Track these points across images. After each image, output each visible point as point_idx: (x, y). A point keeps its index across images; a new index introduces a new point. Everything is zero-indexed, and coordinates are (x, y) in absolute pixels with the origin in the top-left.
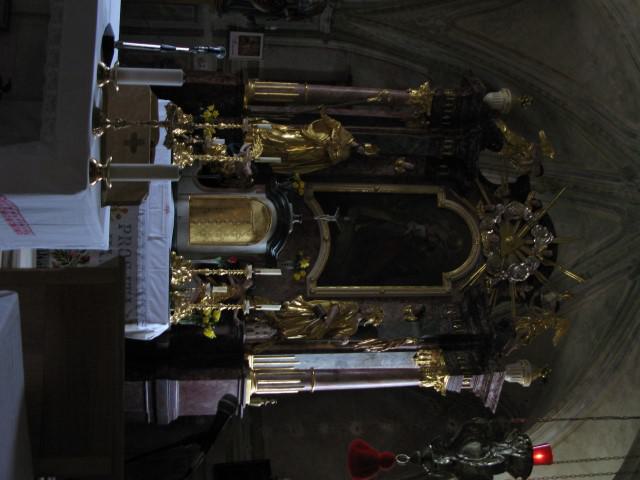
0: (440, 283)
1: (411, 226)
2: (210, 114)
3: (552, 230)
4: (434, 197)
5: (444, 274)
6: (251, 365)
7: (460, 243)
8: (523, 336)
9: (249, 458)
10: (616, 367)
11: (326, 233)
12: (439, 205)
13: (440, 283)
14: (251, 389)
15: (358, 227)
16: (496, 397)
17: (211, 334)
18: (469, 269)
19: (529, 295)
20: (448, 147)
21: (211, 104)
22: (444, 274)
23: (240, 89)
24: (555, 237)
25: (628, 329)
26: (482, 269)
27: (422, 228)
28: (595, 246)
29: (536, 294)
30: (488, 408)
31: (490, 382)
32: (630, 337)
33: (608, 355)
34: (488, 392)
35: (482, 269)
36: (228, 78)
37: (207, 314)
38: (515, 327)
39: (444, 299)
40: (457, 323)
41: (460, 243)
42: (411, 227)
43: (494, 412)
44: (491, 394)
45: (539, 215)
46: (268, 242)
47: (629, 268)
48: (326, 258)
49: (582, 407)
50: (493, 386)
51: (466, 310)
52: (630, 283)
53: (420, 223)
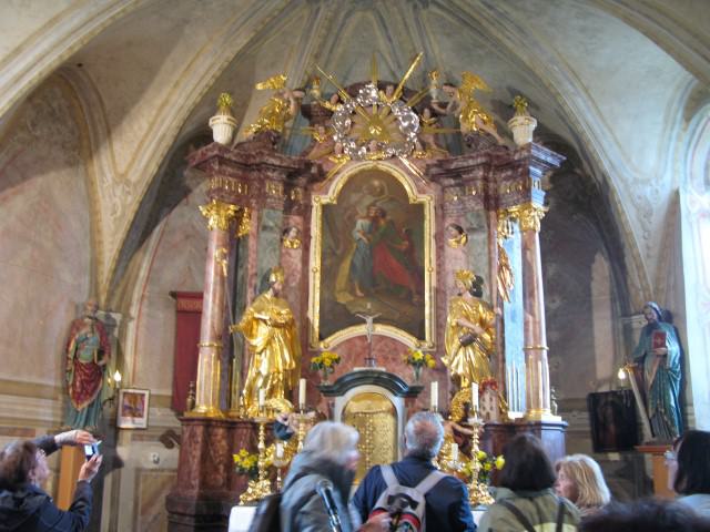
0: (421, 207)
1: (358, 235)
2: (246, 461)
3: (362, 85)
4: (325, 208)
5: (411, 201)
6: (520, 415)
7: (376, 183)
8: (484, 122)
9: (586, 415)
10: (521, 30)
11: (381, 329)
12: (335, 202)
13: (421, 207)
14: (548, 416)
15: (359, 293)
16: (552, 155)
17: (500, 461)
18: (407, 173)
19: (434, 114)
20: (274, 190)
21: (505, 466)
22: (411, 201)
23: (207, 422)
24: (370, 82)
25: (484, 14)
26: (406, 162)
27: (361, 223)
28: (382, 43)
29: (435, 107)
30: (561, 164)
31: (538, 159)
32: (492, 13)
33: (509, 38)
34: (547, 163)
35: (406, 162)
36: (193, 435)
37: (354, 465)
38: (472, 131)
39: (441, 209)
40: (470, 190)
41: (376, 183)
42: (358, 235)
43: (564, 158)
44: (549, 159)
45: (345, 97)
46: (396, 395)
47: (415, 7)
48: (403, 333)
49: (556, 68)
50: (543, 157)
51: (452, 182)
52: (433, 8)
53: (355, 224)
